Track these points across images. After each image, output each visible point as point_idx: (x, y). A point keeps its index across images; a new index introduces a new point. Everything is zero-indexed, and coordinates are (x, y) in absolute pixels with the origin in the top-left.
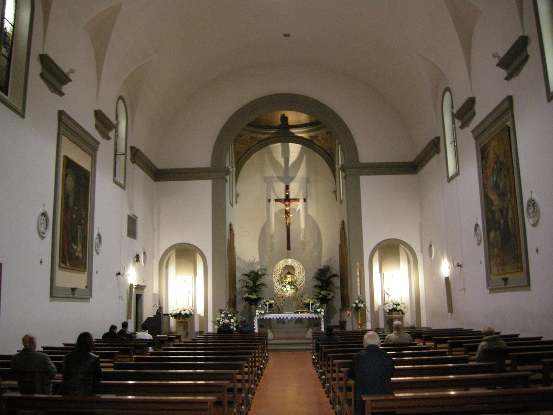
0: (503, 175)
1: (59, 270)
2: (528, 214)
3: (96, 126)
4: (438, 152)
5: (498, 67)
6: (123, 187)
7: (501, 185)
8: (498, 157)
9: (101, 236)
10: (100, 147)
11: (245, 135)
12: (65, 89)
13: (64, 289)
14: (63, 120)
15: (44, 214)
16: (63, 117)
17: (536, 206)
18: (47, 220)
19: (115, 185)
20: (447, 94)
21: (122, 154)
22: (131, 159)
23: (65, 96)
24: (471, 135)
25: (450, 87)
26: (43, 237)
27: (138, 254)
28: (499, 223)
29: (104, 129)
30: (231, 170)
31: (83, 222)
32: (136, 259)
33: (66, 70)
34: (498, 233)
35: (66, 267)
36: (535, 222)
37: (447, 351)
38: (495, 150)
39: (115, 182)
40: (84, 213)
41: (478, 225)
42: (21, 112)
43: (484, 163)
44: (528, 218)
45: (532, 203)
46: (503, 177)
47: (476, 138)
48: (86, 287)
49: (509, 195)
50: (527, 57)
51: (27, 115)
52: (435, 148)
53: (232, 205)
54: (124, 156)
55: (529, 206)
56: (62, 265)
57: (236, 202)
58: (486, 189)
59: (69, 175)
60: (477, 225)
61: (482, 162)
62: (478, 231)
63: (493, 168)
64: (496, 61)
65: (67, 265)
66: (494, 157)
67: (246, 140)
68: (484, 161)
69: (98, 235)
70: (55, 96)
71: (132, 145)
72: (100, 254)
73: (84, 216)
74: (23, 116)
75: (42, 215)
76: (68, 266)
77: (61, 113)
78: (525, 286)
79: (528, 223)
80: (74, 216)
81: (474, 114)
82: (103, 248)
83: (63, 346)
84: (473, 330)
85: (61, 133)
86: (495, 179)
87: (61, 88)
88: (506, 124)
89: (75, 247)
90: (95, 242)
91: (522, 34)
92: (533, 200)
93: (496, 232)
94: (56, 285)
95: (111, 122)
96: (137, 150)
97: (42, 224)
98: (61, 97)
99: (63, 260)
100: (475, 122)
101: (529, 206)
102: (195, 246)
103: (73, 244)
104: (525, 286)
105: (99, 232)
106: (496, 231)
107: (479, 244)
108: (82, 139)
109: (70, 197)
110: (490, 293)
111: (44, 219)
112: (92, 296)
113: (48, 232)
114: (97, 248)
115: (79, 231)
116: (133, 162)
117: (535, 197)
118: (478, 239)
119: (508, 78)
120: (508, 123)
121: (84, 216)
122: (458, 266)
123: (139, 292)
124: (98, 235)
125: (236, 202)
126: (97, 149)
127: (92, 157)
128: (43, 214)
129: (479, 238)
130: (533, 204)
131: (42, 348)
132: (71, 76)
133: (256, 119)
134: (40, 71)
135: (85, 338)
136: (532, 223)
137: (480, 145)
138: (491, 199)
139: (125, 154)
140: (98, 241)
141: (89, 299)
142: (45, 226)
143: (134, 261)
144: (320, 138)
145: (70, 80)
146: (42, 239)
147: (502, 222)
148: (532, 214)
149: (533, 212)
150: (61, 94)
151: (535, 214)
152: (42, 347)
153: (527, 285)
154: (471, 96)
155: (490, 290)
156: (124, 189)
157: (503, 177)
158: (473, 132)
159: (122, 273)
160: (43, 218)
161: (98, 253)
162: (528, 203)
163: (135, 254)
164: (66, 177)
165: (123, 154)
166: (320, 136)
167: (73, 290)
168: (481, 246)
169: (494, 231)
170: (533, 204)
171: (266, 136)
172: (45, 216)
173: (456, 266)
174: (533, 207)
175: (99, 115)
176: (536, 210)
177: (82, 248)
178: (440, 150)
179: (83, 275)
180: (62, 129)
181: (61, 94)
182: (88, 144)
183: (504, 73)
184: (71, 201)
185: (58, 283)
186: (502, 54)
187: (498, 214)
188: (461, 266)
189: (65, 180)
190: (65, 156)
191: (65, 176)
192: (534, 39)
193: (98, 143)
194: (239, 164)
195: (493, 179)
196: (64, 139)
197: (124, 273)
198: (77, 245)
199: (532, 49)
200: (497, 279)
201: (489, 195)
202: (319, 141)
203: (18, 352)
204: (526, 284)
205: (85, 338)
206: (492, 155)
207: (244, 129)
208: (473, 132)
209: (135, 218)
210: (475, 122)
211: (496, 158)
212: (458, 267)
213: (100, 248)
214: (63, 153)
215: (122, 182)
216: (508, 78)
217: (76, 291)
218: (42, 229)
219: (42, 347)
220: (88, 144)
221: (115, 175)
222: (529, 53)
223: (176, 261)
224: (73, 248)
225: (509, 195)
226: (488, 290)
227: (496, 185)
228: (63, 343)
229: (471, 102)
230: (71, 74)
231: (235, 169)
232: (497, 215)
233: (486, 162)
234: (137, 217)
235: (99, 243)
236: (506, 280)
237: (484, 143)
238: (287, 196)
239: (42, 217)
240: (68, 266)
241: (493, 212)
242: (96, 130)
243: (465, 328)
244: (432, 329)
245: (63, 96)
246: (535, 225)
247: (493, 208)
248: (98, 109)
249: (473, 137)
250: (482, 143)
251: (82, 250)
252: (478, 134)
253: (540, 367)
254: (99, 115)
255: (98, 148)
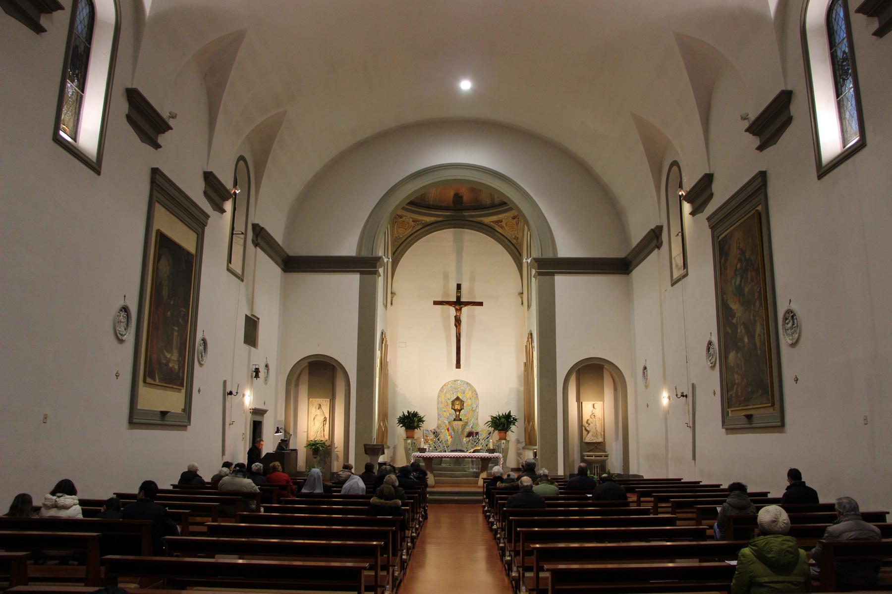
0: (749, 276)
1: (143, 386)
2: (784, 330)
3: (205, 193)
4: (659, 246)
5: (747, 133)
6: (241, 278)
7: (746, 290)
8: (743, 253)
9: (207, 344)
10: (210, 221)
11: (406, 216)
12: (162, 139)
13: (151, 413)
14: (156, 181)
15: (125, 309)
16: (157, 177)
17: (797, 319)
18: (128, 317)
19: (229, 274)
20: (675, 168)
21: (241, 233)
22: (253, 241)
23: (161, 149)
24: (706, 223)
25: (678, 161)
26: (121, 341)
27: (257, 367)
28: (741, 339)
29: (216, 198)
30: (386, 260)
31: (182, 322)
32: (254, 373)
33: (165, 115)
34: (739, 355)
35: (152, 382)
36: (794, 341)
37: (651, 509)
38: (739, 243)
39: (229, 270)
40: (184, 310)
41: (711, 342)
42: (96, 166)
43: (723, 261)
44: (784, 335)
45: (791, 315)
46: (749, 279)
47: (713, 228)
48: (184, 410)
49: (757, 304)
50: (790, 120)
51: (103, 170)
52: (656, 240)
53: (386, 306)
54: (242, 236)
55: (786, 319)
56: (149, 380)
57: (392, 304)
58: (725, 296)
59: (163, 257)
60: (710, 343)
61: (720, 259)
62: (711, 350)
63: (736, 267)
64: (746, 124)
65: (155, 380)
66: (738, 253)
67: (407, 223)
68: (723, 258)
69: (203, 340)
70: (147, 148)
71: (256, 222)
72: (204, 366)
73: (182, 313)
74: (98, 172)
75: (121, 310)
76: (157, 381)
77: (155, 172)
78: (778, 427)
79: (785, 341)
80: (169, 313)
81: (712, 195)
82: (208, 359)
83: (171, 488)
84: (701, 484)
85: (155, 198)
86: (738, 282)
87: (223, 205)
88: (757, 208)
89: (168, 356)
90: (198, 349)
91: (783, 88)
92: (792, 312)
93: (738, 353)
94: (139, 408)
95: (228, 191)
96: (262, 228)
97: (121, 322)
98: (156, 149)
99: (149, 373)
100: (712, 207)
101: (785, 319)
102: (327, 356)
103: (165, 352)
104: (778, 427)
105: (266, 362)
106: (737, 352)
107: (713, 367)
108: (185, 210)
109: (164, 287)
110: (727, 434)
111: (124, 315)
112: (190, 422)
113: (129, 333)
114: (200, 357)
115: (176, 334)
116: (256, 245)
117: (794, 306)
118: (712, 361)
119: (761, 148)
120: (759, 208)
121: (182, 313)
122: (683, 396)
123: (258, 418)
124: (203, 340)
125: (392, 304)
126: (205, 224)
127: (197, 234)
128: (123, 308)
129: (713, 360)
130: (793, 317)
131: (172, 486)
132: (171, 122)
133: (422, 195)
134: (127, 112)
135: (149, 487)
136: (790, 342)
137: (718, 237)
138: (731, 308)
139: (245, 234)
140: (202, 348)
141: (186, 426)
142: (125, 326)
143: (252, 376)
144: (503, 224)
145: (171, 128)
146: (201, 367)
147: (746, 340)
148: (789, 330)
149: (791, 328)
150: (157, 146)
151: (795, 331)
152: (171, 485)
153: (780, 426)
154: (708, 172)
155: (726, 429)
156: (242, 281)
157: (749, 279)
158: (709, 219)
159: (234, 393)
160: (123, 314)
161: (201, 365)
162: (785, 315)
163: (254, 367)
164: (159, 259)
165: (242, 233)
166: (503, 220)
167: (164, 414)
168: (715, 370)
169: (734, 352)
170: (793, 317)
171: (433, 219)
172: (126, 311)
173: (679, 396)
174: (791, 321)
175: (209, 177)
176: (795, 325)
177: (179, 358)
178: (662, 243)
179: (176, 394)
180: (155, 193)
181: (157, 146)
182: (193, 217)
183: (755, 141)
184: (165, 293)
185: (141, 405)
186: (753, 116)
187: (741, 330)
188: (686, 396)
189: (158, 263)
190: (158, 231)
191: (158, 258)
192: (665, 229)
193: (208, 217)
194: (399, 250)
195: (735, 282)
196: (158, 208)
197: (237, 393)
198: (171, 352)
199: (797, 108)
200: (738, 415)
201: (729, 302)
202: (502, 227)
203: (115, 495)
204: (779, 424)
205: (149, 487)
206: (734, 252)
207: (404, 209)
208: (709, 219)
209: (256, 320)
210: (712, 207)
211: (740, 254)
212: (682, 397)
213: (204, 358)
214: (157, 225)
215: (239, 271)
216: (761, 148)
217: (168, 416)
218: (121, 328)
219: (171, 485)
220: (193, 217)
221: (230, 260)
222: (713, 191)
223: (309, 379)
224: (165, 356)
225: (757, 304)
226: (724, 430)
227: (739, 290)
228: (172, 484)
229: (708, 179)
230: (171, 119)
231: (391, 260)
232: (739, 331)
233: (726, 260)
234: (258, 319)
235: (203, 351)
236: (749, 417)
237: (723, 236)
238: (458, 298)
239: (121, 312)
240: (157, 381)
241: (734, 327)
242: (204, 198)
243: (646, 477)
244: (645, 478)
245: (159, 149)
246: (793, 345)
247: (734, 321)
248: (209, 170)
249: (709, 226)
250: (720, 235)
251: (178, 360)
252: (716, 223)
253: (670, 505)
254: (209, 177)
255: (207, 223)
